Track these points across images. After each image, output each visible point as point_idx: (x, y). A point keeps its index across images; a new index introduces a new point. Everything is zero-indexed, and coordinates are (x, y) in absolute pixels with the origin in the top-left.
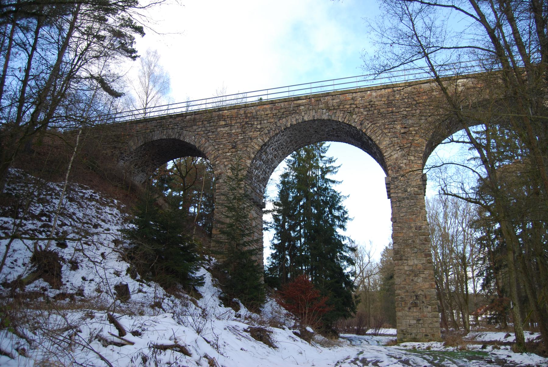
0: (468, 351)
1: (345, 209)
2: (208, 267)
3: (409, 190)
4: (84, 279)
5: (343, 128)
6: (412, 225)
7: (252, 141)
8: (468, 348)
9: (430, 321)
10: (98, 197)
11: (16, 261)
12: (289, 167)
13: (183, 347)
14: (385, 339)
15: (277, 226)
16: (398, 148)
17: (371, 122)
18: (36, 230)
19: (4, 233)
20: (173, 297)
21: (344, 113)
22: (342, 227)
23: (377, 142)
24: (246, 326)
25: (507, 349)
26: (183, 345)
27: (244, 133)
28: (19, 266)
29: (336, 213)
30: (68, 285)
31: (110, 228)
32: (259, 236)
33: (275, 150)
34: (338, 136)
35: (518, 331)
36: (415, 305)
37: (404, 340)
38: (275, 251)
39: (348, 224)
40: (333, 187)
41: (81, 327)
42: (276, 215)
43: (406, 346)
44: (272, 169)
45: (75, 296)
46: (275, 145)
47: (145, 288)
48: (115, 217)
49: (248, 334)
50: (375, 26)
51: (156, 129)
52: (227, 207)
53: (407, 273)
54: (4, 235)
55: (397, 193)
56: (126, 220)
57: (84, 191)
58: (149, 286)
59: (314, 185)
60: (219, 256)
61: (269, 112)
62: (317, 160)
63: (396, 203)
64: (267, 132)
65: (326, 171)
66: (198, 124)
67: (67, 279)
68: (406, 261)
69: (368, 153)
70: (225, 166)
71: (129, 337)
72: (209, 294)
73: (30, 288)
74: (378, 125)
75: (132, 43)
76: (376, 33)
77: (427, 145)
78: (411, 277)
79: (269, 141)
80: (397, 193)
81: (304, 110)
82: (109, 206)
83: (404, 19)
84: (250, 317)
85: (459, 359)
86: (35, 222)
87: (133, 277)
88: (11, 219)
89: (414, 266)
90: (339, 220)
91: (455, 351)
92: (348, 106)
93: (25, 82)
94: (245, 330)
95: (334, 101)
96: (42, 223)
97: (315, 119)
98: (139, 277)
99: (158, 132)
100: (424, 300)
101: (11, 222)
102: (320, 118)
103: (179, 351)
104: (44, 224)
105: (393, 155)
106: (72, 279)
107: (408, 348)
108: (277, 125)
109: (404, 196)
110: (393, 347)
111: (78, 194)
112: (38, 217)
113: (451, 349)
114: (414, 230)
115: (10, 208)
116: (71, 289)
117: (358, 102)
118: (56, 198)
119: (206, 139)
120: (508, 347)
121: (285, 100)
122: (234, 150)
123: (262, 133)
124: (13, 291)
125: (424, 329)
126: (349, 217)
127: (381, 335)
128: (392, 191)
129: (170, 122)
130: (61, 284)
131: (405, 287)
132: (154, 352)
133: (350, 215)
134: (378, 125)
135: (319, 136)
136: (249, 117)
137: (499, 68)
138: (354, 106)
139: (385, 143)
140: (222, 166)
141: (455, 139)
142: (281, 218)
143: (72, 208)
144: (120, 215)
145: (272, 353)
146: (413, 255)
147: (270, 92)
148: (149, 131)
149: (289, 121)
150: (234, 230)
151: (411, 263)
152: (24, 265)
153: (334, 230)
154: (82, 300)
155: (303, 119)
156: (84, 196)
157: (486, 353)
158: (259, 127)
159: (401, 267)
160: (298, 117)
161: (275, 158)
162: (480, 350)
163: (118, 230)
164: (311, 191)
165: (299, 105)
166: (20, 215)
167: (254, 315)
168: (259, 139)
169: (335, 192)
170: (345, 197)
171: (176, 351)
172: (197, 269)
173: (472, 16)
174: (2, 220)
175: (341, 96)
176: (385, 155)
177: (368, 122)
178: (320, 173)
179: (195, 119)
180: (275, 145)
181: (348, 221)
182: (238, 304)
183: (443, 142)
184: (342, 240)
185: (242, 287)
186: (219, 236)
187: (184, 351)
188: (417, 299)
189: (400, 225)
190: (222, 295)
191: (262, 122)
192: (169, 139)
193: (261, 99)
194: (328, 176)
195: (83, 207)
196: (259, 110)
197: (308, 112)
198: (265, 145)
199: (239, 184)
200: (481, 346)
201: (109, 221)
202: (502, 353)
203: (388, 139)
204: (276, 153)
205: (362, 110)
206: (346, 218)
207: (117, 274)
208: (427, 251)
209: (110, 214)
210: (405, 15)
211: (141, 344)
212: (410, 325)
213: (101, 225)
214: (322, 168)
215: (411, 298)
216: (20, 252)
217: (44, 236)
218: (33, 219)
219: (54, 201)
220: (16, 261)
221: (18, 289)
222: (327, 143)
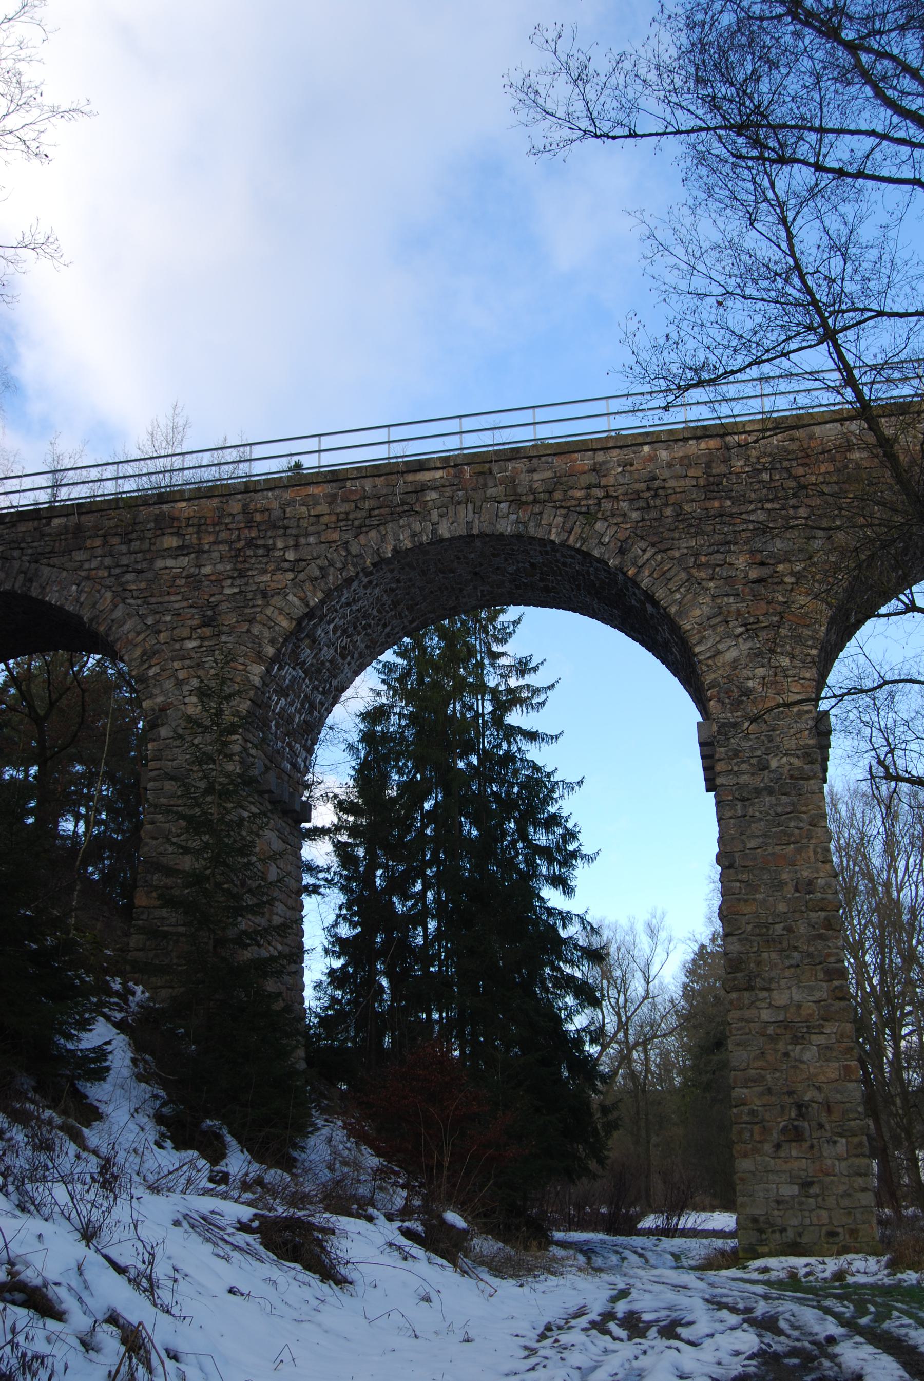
1: (570, 825)
2: (119, 1016)
3: (774, 764)
5: (564, 564)
6: (785, 876)
7: (268, 604)
9: (841, 1189)
12: (390, 687)
13: (37, 1289)
14: (697, 1248)
15: (347, 878)
16: (740, 630)
21: (566, 516)
22: (562, 883)
23: (673, 610)
24: (245, 1213)
26: (38, 1282)
27: (241, 576)
29: (542, 839)
32: (289, 914)
33: (345, 631)
34: (547, 590)
36: (795, 1135)
37: (760, 1249)
39: (580, 874)
40: (534, 753)
43: (766, 1270)
44: (334, 695)
46: (344, 616)
52: (181, 816)
53: (770, 1031)
55: (737, 774)
59: (469, 748)
61: (323, 508)
62: (480, 665)
63: (733, 807)
64: (317, 573)
65: (509, 700)
68: (765, 994)
69: (642, 643)
70: (179, 683)
74: (677, 554)
76: (672, 261)
77: (832, 621)
78: (781, 1046)
79: (322, 602)
84: (259, 1182)
89: (793, 1010)
90: (551, 861)
92: (579, 494)
94: (243, 1227)
95: (536, 476)
97: (475, 531)
100: (824, 1118)
105: (726, 653)
107: (773, 1275)
108: (349, 553)
114: (789, 892)
119: (116, 594)
122: (207, 631)
123: (302, 576)
125: (824, 1214)
126: (584, 850)
131: (763, 1078)
133: (586, 843)
134: (677, 554)
136: (259, 524)
138: (599, 493)
139: (697, 612)
140: (169, 685)
146: (787, 973)
149: (390, 537)
151: (780, 998)
155: (434, 532)
158: (290, 556)
160: (417, 527)
161: (343, 657)
165: (423, 488)
167: (273, 1175)
168: (290, 597)
169: (536, 768)
170: (570, 786)
171: (14, 1303)
172: (85, 1025)
175: (557, 461)
176: (697, 650)
177: (643, 544)
178: (489, 708)
179: (78, 530)
180: (344, 616)
184: (559, 923)
185: (237, 1082)
188: (800, 1115)
189: (744, 877)
191: (302, 540)
193: (298, 466)
194: (514, 718)
197: (451, 509)
198: (310, 614)
203: (708, 600)
204: (346, 641)
205: (624, 505)
206: (574, 855)
208: (832, 959)
212: (778, 1202)
214: (495, 692)
222: (512, 612)
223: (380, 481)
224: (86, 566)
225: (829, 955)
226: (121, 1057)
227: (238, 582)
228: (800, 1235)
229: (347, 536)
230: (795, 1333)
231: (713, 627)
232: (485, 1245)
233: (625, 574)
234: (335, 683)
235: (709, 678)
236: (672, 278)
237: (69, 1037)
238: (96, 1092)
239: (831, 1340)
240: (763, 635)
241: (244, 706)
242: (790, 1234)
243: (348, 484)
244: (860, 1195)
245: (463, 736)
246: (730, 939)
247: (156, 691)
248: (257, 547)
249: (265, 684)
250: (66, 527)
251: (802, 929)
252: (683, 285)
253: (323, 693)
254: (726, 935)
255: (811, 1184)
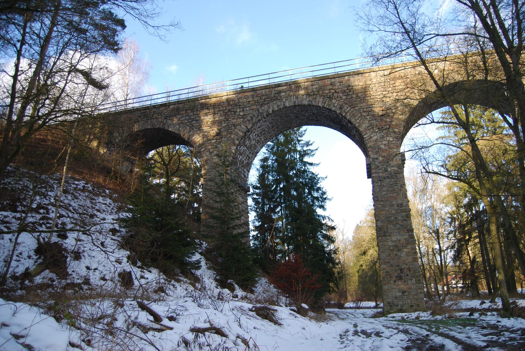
0: (457, 319)
1: (324, 190)
2: (200, 251)
3: (389, 170)
4: (88, 268)
5: (323, 113)
6: (394, 203)
7: (236, 128)
8: (456, 316)
9: (414, 293)
10: (91, 188)
11: (21, 254)
12: (269, 151)
13: (219, 329)
14: (370, 312)
15: (257, 208)
16: (377, 130)
17: (350, 106)
18: (35, 222)
19: (5, 227)
20: (173, 282)
21: (323, 99)
22: (322, 207)
23: (357, 125)
24: (250, 306)
25: (494, 315)
26: (219, 327)
27: (227, 120)
28: (25, 259)
29: (316, 195)
30: (74, 275)
31: (106, 217)
32: (245, 219)
33: (258, 135)
34: (317, 121)
35: (504, 298)
36: (400, 278)
37: (391, 311)
38: (256, 233)
39: (328, 204)
40: (312, 169)
41: (117, 317)
42: (256, 198)
43: (394, 317)
44: (255, 154)
45: (83, 285)
46: (258, 131)
47: (147, 275)
48: (109, 206)
49: (254, 313)
50: (362, 14)
51: (140, 120)
52: (215, 192)
53: (391, 248)
54: (6, 230)
55: (378, 173)
56: (120, 209)
57: (76, 183)
58: (150, 272)
59: (293, 168)
60: (210, 240)
61: (250, 99)
62: (296, 144)
63: (377, 183)
64: (250, 118)
65: (304, 154)
66: (181, 113)
67: (72, 270)
68: (389, 237)
69: (346, 135)
70: (211, 153)
71: (166, 322)
72: (207, 276)
73: (38, 279)
74: (357, 108)
75: (114, 36)
76: (363, 21)
77: (404, 127)
78: (395, 252)
79: (252, 127)
80: (378, 173)
81: (285, 96)
82: (102, 196)
83: (390, 7)
84: (246, 297)
85: (453, 326)
86: (34, 215)
87: (134, 264)
88: (10, 213)
89: (398, 242)
90: (318, 200)
91: (444, 319)
92: (327, 92)
93: (15, 78)
94: (251, 310)
95: (314, 87)
96: (41, 216)
97: (296, 104)
98: (139, 264)
99: (142, 122)
100: (408, 273)
101: (11, 216)
102: (300, 104)
103: (215, 333)
104: (43, 216)
105: (372, 137)
106: (77, 269)
107: (397, 318)
108: (259, 112)
109: (384, 175)
110: (381, 318)
111: (71, 186)
112: (36, 210)
113: (439, 317)
114: (395, 207)
115: (8, 202)
116: (78, 279)
117: (337, 87)
118: (51, 191)
119: (190, 127)
120: (495, 313)
121: (266, 87)
122: (218, 137)
123: (245, 120)
124: (22, 283)
125: (409, 300)
126: (328, 198)
127: (362, 308)
128: (373, 171)
129: (154, 112)
130: (67, 274)
131: (390, 262)
132: (197, 336)
133: (328, 195)
134: (357, 108)
135: (300, 121)
136: (232, 105)
137: (479, 52)
138: (333, 91)
139: (364, 125)
140: (208, 153)
141: (435, 121)
142: (260, 200)
143: (67, 199)
144: (113, 204)
145: (279, 330)
146: (396, 231)
147: (251, 80)
148: (133, 121)
149: (271, 107)
150: (224, 214)
151: (394, 238)
152: (29, 257)
153: (315, 211)
154: (89, 289)
155: (284, 105)
156: (77, 187)
157: (475, 320)
158: (242, 114)
159: (386, 243)
160: (279, 103)
161: (258, 143)
162: (468, 317)
163: (113, 219)
164: (291, 174)
165: (280, 92)
166: (18, 209)
167: (249, 295)
168: (242, 126)
169: (313, 174)
170: (323, 178)
171: (212, 333)
172: (193, 254)
173: (465, 4)
174: (2, 215)
175: (320, 82)
176: (365, 137)
177: (347, 106)
178: (298, 156)
179: (178, 109)
180: (258, 131)
181: (327, 201)
182: (233, 285)
183: (420, 122)
184: (322, 219)
185: (237, 268)
186: (208, 220)
187: (219, 332)
188: (401, 272)
189: (382, 203)
190: (218, 277)
191: (245, 109)
192: (155, 127)
193: (242, 87)
194: (306, 159)
195: (77, 199)
196: (241, 98)
197: (289, 98)
198: (248, 131)
199: (227, 170)
200: (468, 313)
201: (104, 211)
202: (491, 319)
203: (367, 122)
204: (258, 138)
205: (341, 94)
206: (325, 199)
207: (119, 261)
208: (409, 226)
209: (103, 204)
210: (390, 3)
211: (182, 328)
212: (396, 298)
213: (96, 215)
214: (300, 152)
215: (396, 272)
216: (23, 245)
217: (44, 228)
218: (31, 212)
219: (49, 193)
220: (21, 254)
221: (27, 281)
222: (304, 128)
223: (267, 90)
224: (181, 119)
225: (408, 225)
226: (203, 263)
227: (226, 122)
228: (402, 307)
229: (258, 107)
230: (416, 334)
231: (369, 130)
232: (312, 314)
233: (342, 115)
234: (255, 151)
235: (369, 145)
236: (363, 26)
237: (189, 257)
238: (198, 273)
239: (427, 335)
240: (384, 132)
241: (231, 159)
242: (399, 307)
243: (258, 92)
244: (420, 295)
245: (292, 164)
246: (378, 222)
247: (204, 155)
248: (232, 111)
249: (236, 152)
250: (174, 108)
251: (400, 218)
252: (366, 28)
253: (252, 154)
254: (377, 221)
255: (405, 292)
